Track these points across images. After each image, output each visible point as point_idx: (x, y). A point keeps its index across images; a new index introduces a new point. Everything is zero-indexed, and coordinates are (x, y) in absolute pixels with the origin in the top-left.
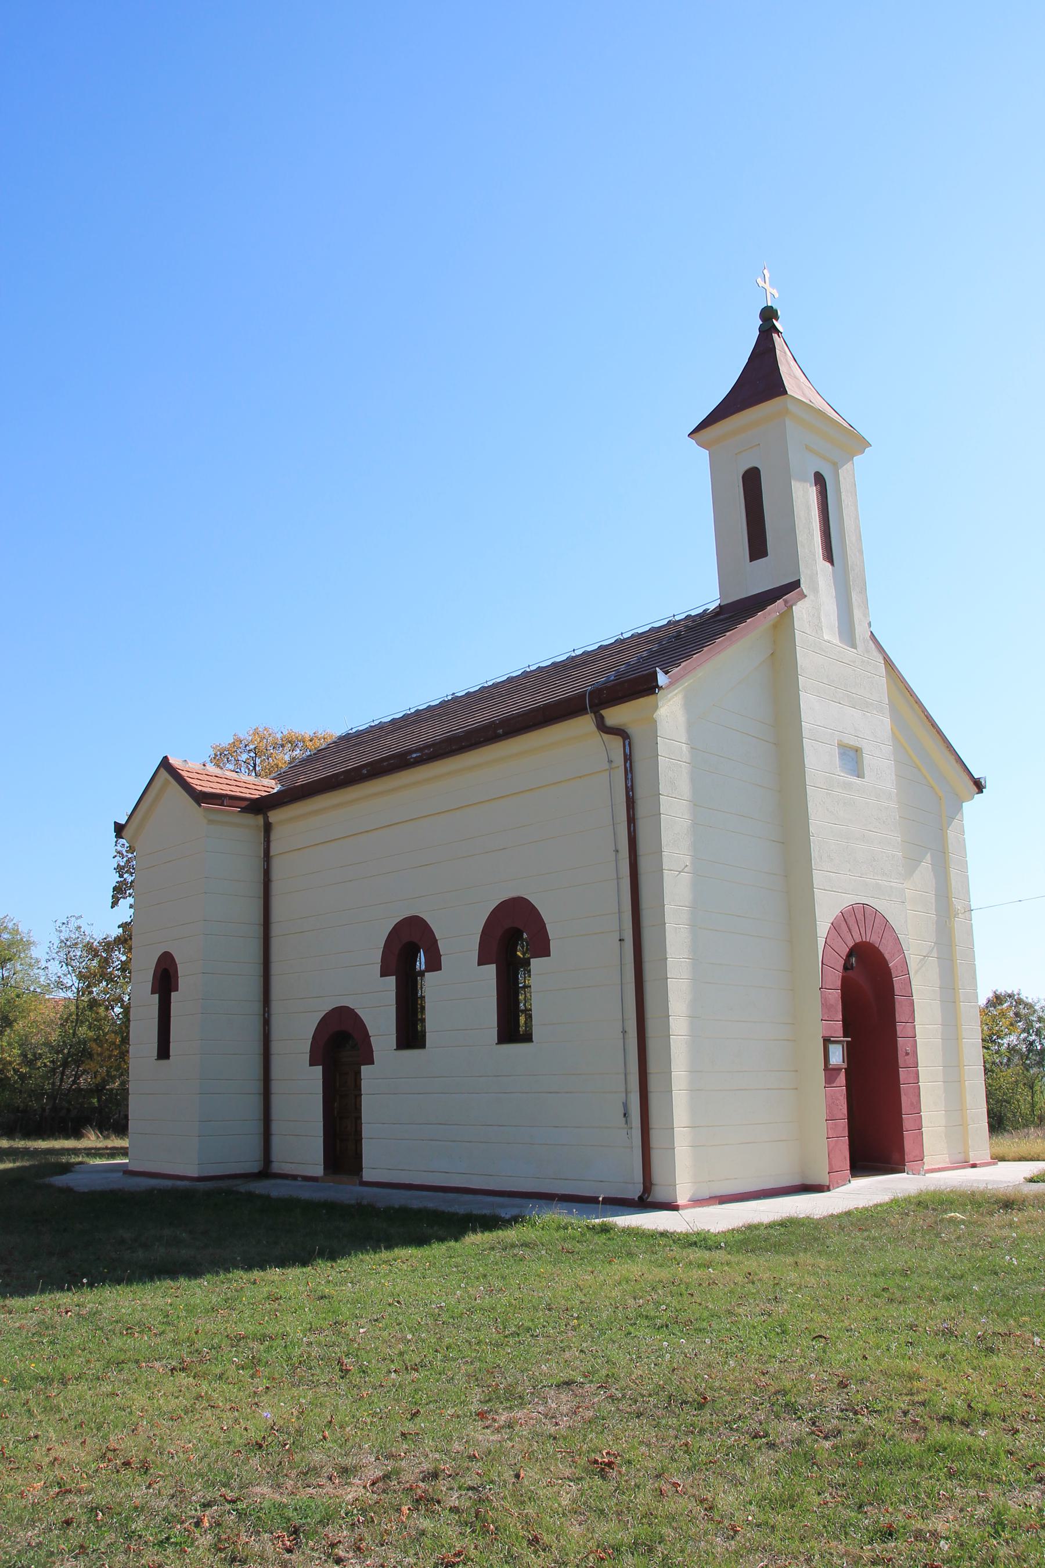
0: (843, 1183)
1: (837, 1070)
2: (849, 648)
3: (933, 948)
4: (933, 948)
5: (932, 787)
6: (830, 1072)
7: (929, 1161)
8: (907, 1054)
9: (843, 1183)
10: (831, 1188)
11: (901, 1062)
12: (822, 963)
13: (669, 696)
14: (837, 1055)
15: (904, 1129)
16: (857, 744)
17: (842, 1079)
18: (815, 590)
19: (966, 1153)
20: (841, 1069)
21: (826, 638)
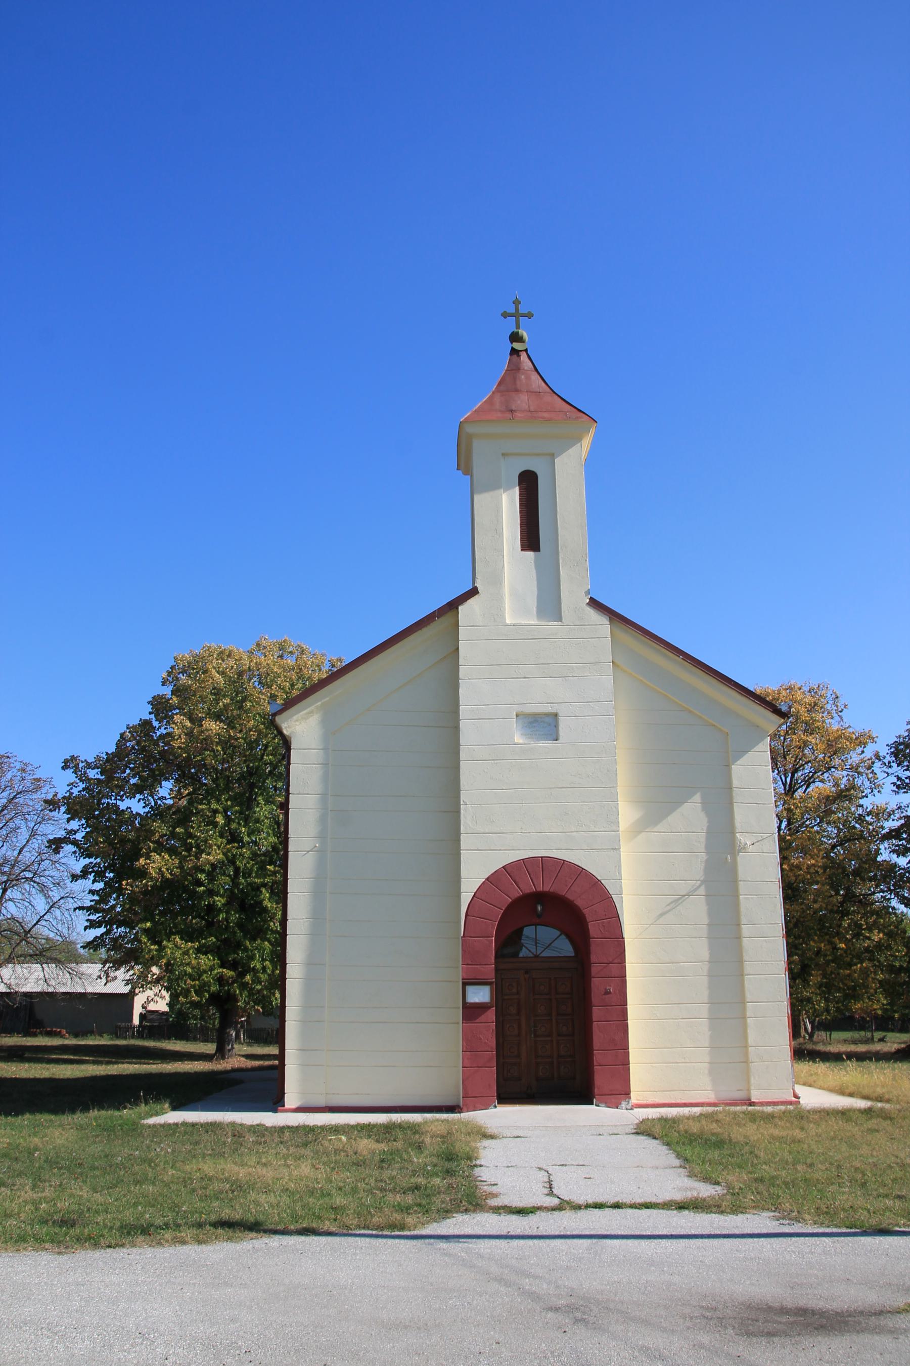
0: (484, 1108)
1: (480, 1008)
2: (550, 623)
3: (700, 886)
4: (700, 886)
5: (714, 725)
6: (471, 1012)
7: (635, 1098)
8: (607, 993)
9: (484, 1108)
10: (465, 1108)
11: (595, 1000)
12: (467, 915)
13: (295, 718)
14: (480, 995)
15: (595, 1063)
16: (554, 711)
17: (491, 1015)
18: (497, 580)
19: (749, 1090)
20: (490, 1008)
21: (508, 621)
